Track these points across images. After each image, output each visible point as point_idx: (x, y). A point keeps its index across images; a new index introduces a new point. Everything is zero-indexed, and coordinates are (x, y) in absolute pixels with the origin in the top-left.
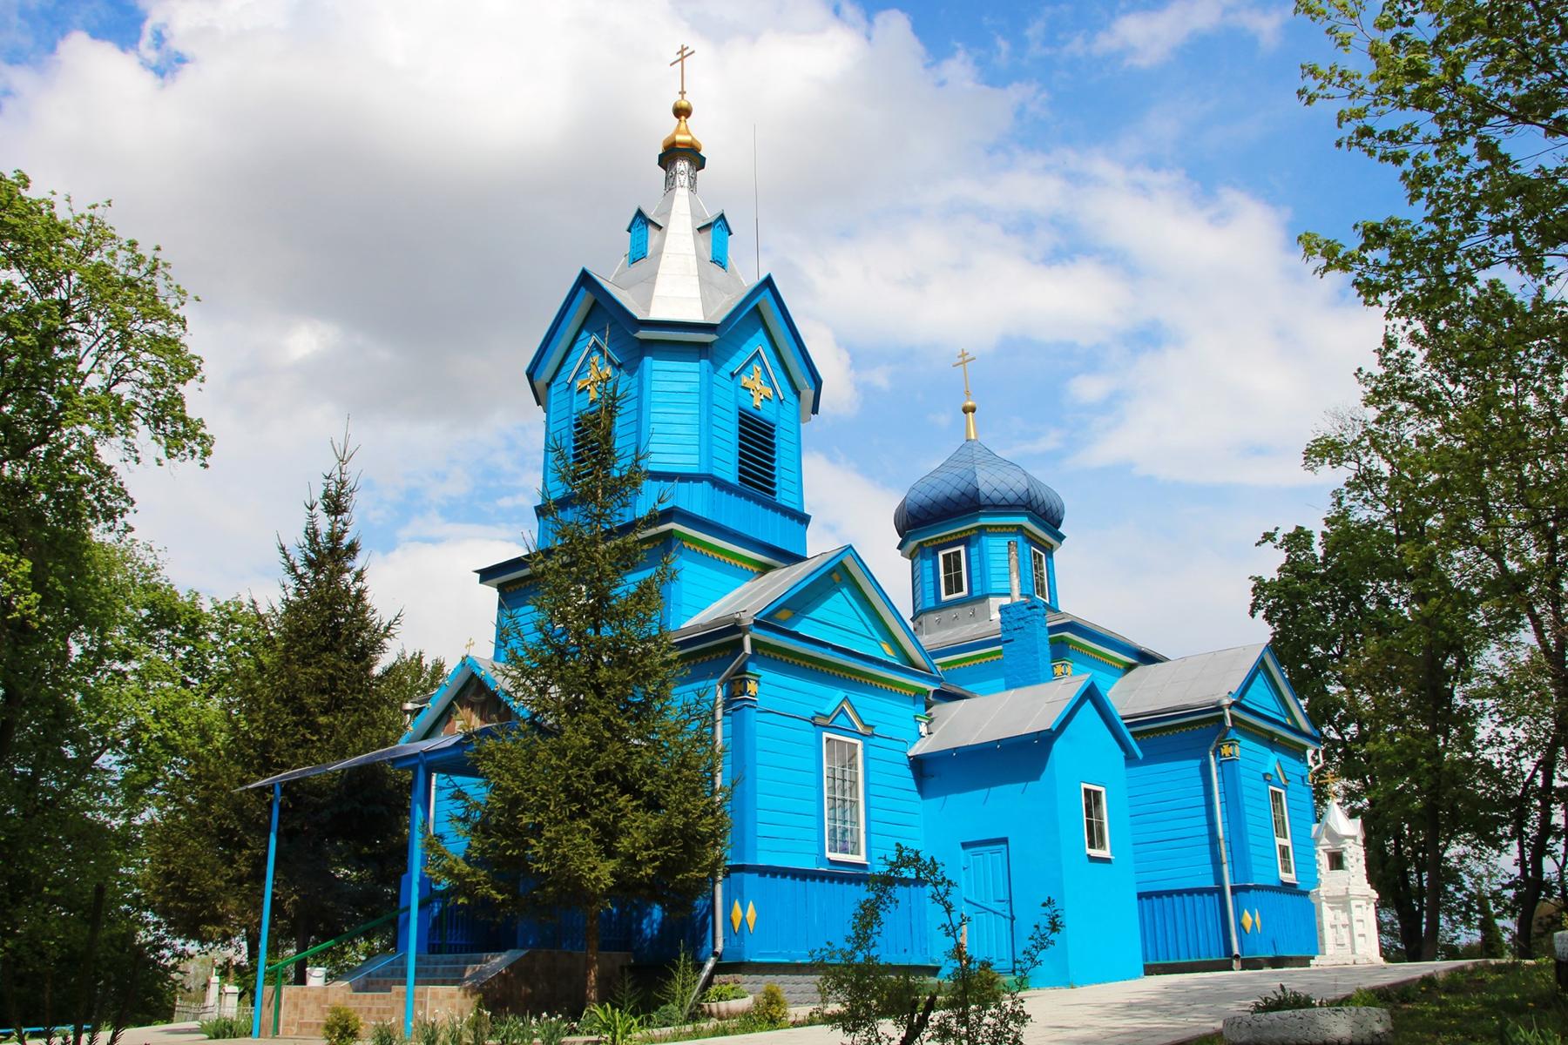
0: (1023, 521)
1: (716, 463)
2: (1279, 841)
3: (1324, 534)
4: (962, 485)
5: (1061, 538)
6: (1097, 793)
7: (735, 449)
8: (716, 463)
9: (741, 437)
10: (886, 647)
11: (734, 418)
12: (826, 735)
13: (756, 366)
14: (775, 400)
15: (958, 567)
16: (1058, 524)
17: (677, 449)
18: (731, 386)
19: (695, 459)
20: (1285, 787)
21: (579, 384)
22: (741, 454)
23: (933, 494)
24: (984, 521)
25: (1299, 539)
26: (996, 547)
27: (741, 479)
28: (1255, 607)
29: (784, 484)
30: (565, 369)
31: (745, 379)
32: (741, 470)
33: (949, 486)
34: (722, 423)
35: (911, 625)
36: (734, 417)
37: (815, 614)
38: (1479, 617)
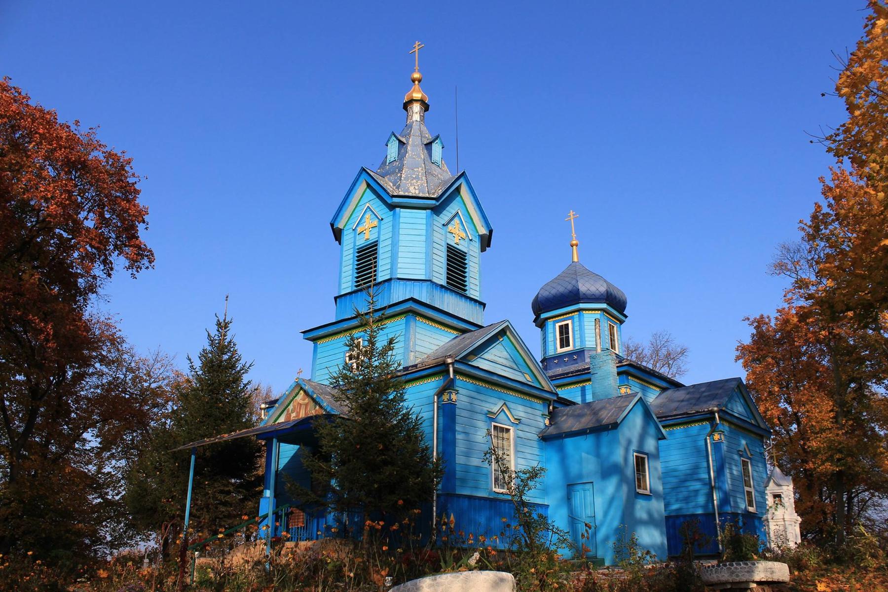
0: (604, 306)
1: (435, 274)
2: (747, 489)
3: (776, 318)
4: (570, 287)
5: (626, 317)
6: (643, 459)
7: (445, 266)
8: (435, 274)
9: (448, 260)
10: (527, 376)
11: (444, 249)
12: (493, 424)
13: (456, 220)
14: (467, 239)
15: (561, 340)
16: (624, 308)
17: (410, 255)
18: (443, 232)
19: (423, 272)
20: (750, 459)
21: (359, 230)
22: (448, 269)
23: (554, 292)
24: (582, 306)
25: (760, 323)
26: (589, 319)
27: (448, 283)
28: (738, 358)
29: (471, 264)
30: (353, 216)
31: (450, 227)
32: (448, 278)
33: (561, 289)
34: (438, 263)
35: (541, 364)
36: (444, 249)
37: (486, 356)
38: (345, 518)
